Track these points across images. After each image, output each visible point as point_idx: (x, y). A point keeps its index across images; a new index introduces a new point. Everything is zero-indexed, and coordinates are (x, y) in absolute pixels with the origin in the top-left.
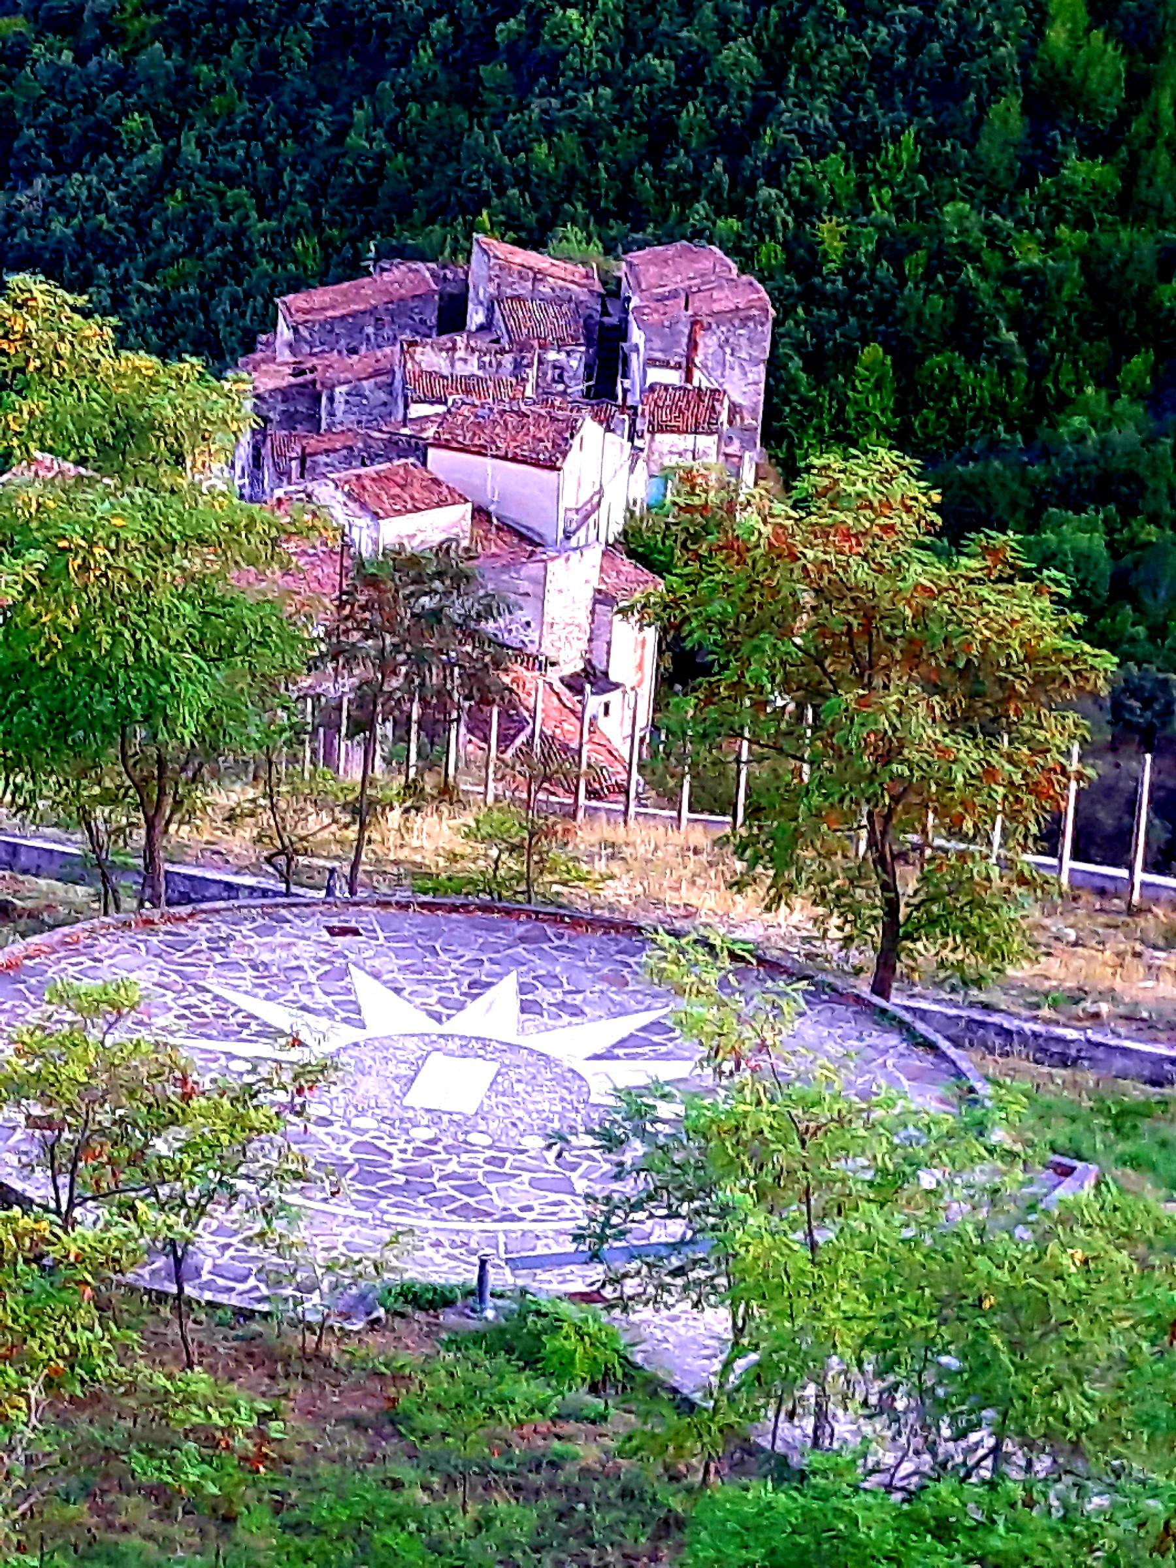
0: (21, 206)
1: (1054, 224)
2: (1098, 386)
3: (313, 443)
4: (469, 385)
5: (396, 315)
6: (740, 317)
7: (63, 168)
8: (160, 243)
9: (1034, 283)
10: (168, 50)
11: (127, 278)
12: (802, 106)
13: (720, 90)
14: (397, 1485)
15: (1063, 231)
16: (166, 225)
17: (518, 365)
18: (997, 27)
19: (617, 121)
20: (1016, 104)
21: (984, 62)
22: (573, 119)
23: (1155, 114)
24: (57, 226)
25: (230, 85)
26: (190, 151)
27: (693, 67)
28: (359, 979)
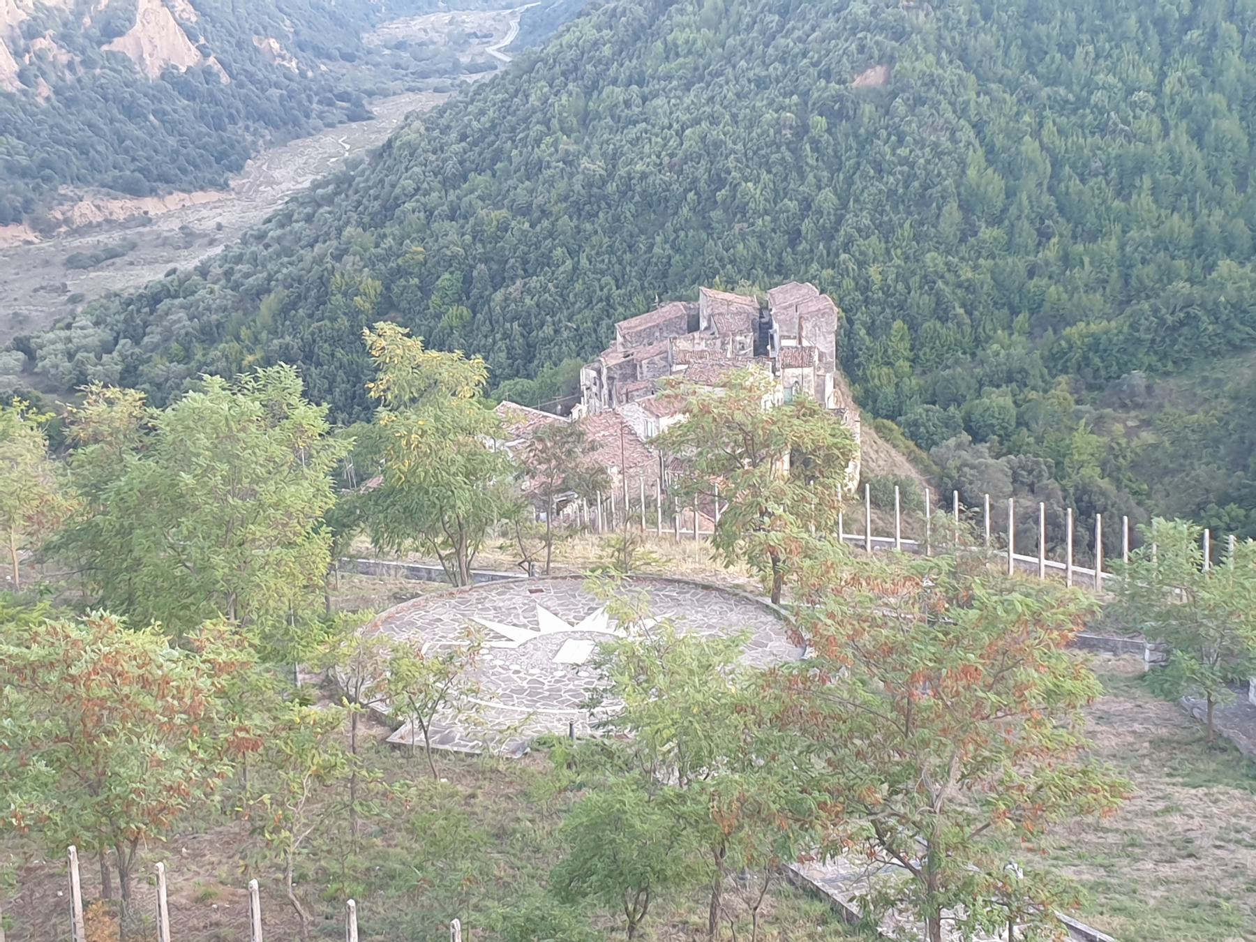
0: (510, 294)
1: (977, 258)
2: (1003, 329)
3: (631, 387)
4: (701, 355)
5: (669, 326)
6: (821, 313)
7: (527, 274)
8: (573, 304)
9: (969, 287)
10: (571, 217)
11: (560, 321)
12: (856, 216)
13: (820, 212)
14: (518, 820)
15: (981, 261)
16: (575, 295)
17: (723, 344)
18: (943, 172)
19: (774, 230)
20: (955, 205)
21: (939, 188)
22: (754, 231)
23: (1020, 204)
24: (528, 301)
25: (599, 231)
26: (584, 262)
27: (807, 204)
28: (540, 610)
